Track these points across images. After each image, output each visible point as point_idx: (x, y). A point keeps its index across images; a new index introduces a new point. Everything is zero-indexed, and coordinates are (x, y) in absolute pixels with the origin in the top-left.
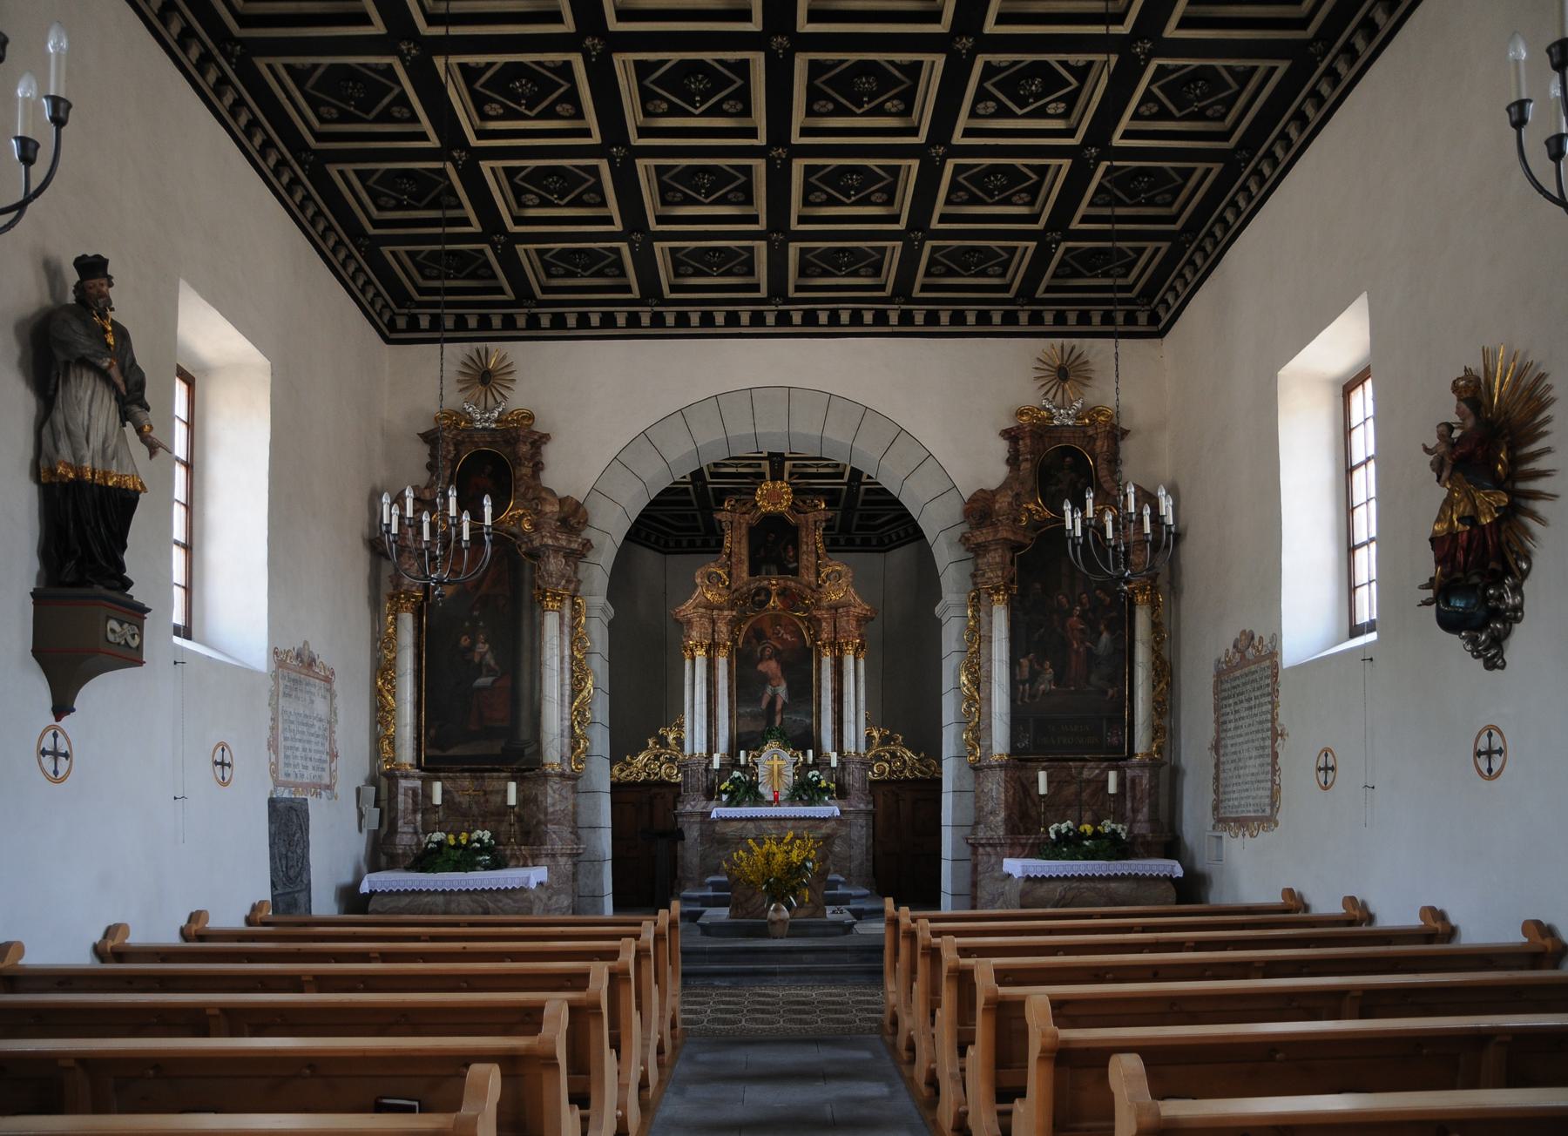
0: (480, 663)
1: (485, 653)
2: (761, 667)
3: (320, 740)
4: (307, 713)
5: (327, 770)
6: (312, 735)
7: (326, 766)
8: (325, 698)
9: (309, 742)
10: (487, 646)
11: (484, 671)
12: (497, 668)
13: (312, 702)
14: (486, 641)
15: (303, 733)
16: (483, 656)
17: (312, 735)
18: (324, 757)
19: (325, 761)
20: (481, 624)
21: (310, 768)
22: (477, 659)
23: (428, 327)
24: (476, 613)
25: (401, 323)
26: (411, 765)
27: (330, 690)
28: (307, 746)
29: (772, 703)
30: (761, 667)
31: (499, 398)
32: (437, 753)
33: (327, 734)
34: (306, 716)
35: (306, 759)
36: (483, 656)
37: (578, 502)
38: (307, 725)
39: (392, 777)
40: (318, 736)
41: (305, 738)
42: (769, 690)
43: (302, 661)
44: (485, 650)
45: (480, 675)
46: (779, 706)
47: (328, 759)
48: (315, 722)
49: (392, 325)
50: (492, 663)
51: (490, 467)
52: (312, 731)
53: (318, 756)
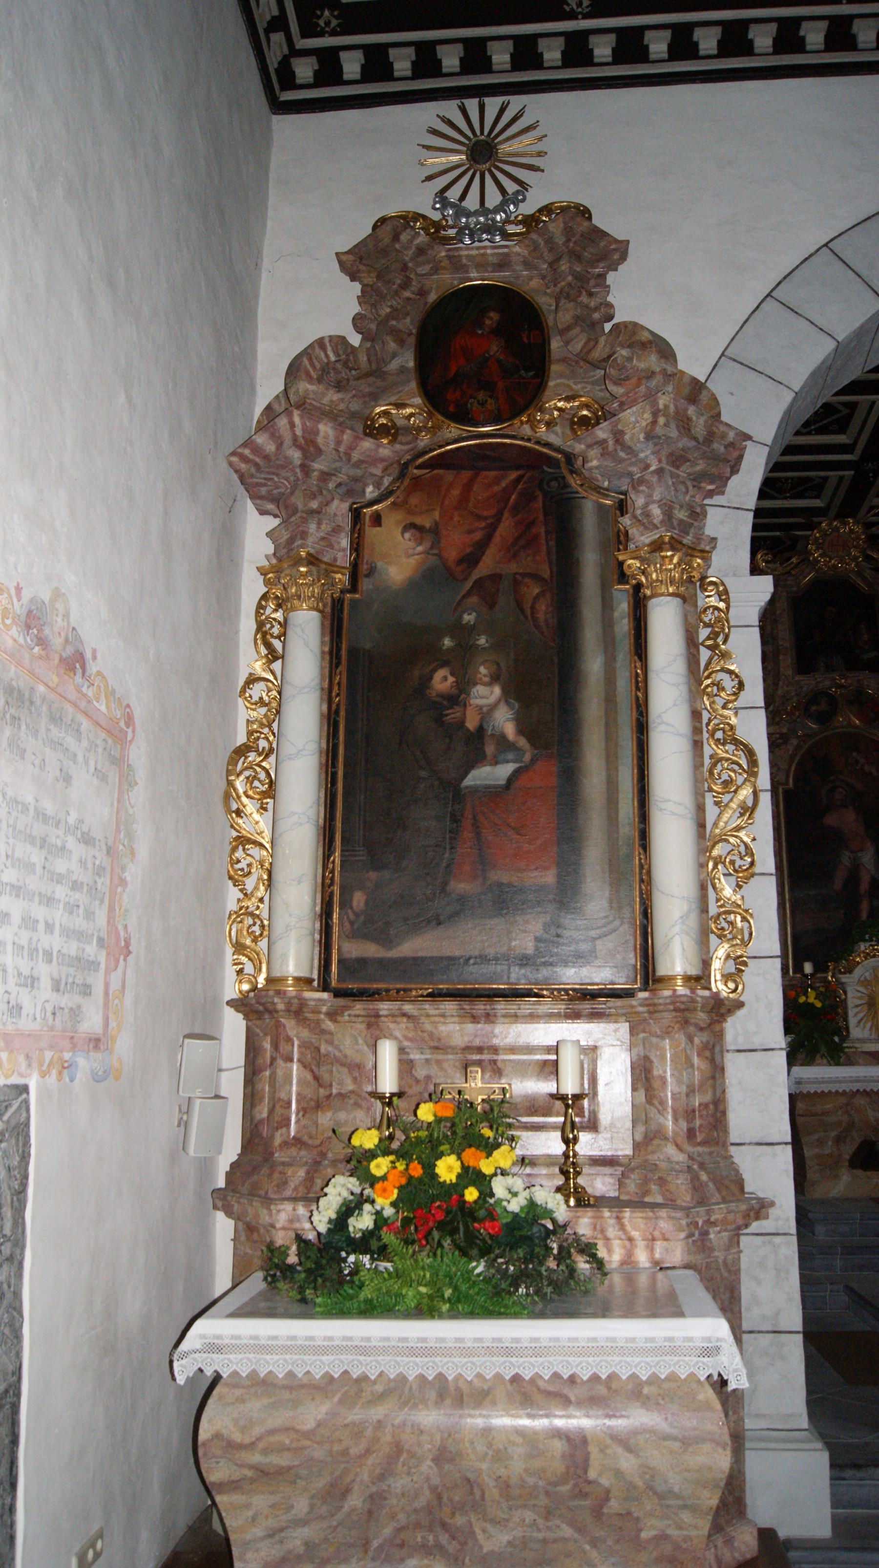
0: (481, 729)
1: (494, 707)
2: (830, 820)
3: (80, 897)
4: (49, 806)
5: (98, 990)
6: (58, 879)
7: (97, 981)
8: (104, 779)
9: (49, 901)
10: (497, 690)
11: (490, 749)
12: (522, 742)
13: (68, 779)
14: (495, 678)
15: (30, 868)
16: (486, 714)
17: (58, 879)
18: (91, 950)
19: (94, 965)
20: (482, 641)
21: (46, 983)
22: (471, 724)
23: (358, 76)
24: (468, 618)
25: (304, 70)
26: (304, 982)
27: (119, 761)
28: (40, 912)
29: (853, 877)
30: (830, 820)
31: (511, 187)
32: (371, 950)
33: (103, 884)
34: (41, 816)
35: (33, 952)
36: (486, 714)
37: (695, 381)
38: (43, 843)
39: (496, 1070)
40: (76, 886)
41: (33, 883)
42: (846, 859)
43: (42, 641)
44: (493, 699)
45: (476, 758)
46: (864, 886)
47: (102, 959)
48: (71, 843)
49: (288, 80)
50: (510, 730)
51: (494, 316)
52: (60, 866)
53: (72, 948)
